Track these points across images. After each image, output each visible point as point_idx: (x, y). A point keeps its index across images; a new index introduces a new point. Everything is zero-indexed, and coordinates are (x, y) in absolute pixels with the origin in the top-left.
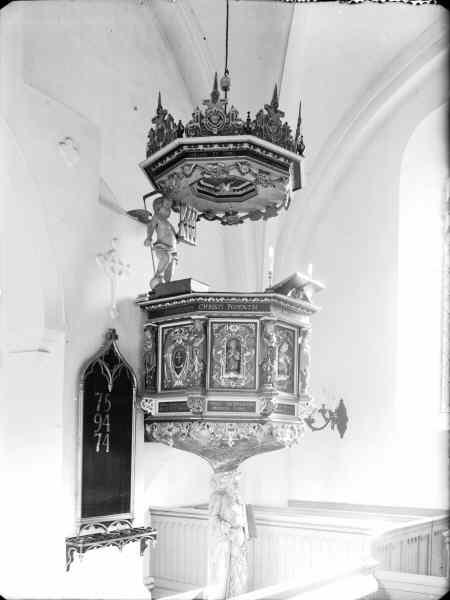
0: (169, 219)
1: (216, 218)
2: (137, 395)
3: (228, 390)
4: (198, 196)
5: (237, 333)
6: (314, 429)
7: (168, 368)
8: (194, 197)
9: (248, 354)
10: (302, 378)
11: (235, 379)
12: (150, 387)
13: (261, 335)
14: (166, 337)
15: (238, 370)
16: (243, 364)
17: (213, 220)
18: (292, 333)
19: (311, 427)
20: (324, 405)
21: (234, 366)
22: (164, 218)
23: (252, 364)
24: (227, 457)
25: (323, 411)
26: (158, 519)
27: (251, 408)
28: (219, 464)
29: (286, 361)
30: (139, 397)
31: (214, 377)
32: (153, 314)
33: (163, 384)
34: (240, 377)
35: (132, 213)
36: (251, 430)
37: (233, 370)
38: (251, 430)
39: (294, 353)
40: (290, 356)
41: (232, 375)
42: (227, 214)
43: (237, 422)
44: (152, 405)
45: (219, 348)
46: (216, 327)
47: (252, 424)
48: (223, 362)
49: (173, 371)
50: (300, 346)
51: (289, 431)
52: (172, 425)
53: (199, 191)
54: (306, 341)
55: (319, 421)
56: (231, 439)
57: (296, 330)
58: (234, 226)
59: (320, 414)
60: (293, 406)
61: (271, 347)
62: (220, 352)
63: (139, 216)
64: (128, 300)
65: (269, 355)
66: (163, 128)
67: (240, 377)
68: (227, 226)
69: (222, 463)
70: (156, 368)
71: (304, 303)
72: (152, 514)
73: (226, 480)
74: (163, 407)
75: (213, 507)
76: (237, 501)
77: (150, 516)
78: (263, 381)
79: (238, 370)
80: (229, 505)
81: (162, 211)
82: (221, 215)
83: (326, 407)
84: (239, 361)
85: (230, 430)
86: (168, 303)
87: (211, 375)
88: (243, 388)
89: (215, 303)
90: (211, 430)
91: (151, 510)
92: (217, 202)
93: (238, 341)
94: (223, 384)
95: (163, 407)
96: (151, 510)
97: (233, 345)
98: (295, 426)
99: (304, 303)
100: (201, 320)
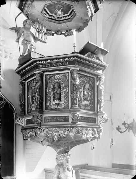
0: (30, 30)
1: (62, 34)
2: (16, 117)
3: (55, 110)
4: (49, 21)
5: (59, 79)
6: (121, 132)
7: (30, 102)
8: (47, 22)
9: (65, 90)
10: (99, 102)
11: (58, 104)
12: (23, 114)
13: (71, 79)
14: (28, 87)
15: (60, 99)
16: (63, 96)
17: (60, 35)
18: (92, 80)
19: (119, 131)
20: (124, 121)
21: (58, 97)
22: (28, 29)
23: (67, 96)
24: (64, 145)
25: (124, 124)
26: (48, 174)
27: (66, 119)
28: (59, 150)
29: (88, 93)
30: (16, 117)
31: (48, 104)
32: (22, 76)
33: (28, 110)
34: (62, 103)
35: (12, 29)
36: (67, 132)
37: (57, 99)
38: (67, 132)
39: (94, 90)
40: (91, 91)
41: (56, 102)
42: (67, 31)
43: (59, 127)
44: (22, 122)
45: (50, 88)
46: (48, 77)
47: (67, 129)
48: (52, 96)
49: (31, 104)
50: (98, 86)
51: (91, 132)
52: (29, 131)
53: (49, 18)
54: (101, 83)
55: (123, 129)
56: (56, 137)
57: (95, 77)
58: (70, 36)
59: (123, 125)
60: (95, 118)
61: (76, 84)
62: (50, 91)
63: (16, 29)
64: (11, 71)
65: (75, 88)
66: (73, 34)
67: (62, 103)
68: (67, 37)
69: (60, 150)
70: (25, 102)
71: (97, 61)
72: (45, 172)
73: (62, 159)
74: (28, 122)
75: (55, 173)
76: (68, 169)
77: (45, 173)
78: (73, 104)
79: (60, 99)
80: (64, 171)
81: (27, 26)
82: (64, 33)
83: (125, 122)
84: (60, 94)
85: (56, 132)
86: (27, 66)
87: (46, 102)
88: (63, 108)
89: (46, 64)
90: (45, 132)
91: (45, 170)
92: (60, 24)
93: (59, 83)
94: (52, 107)
95: (28, 122)
96: (45, 170)
97: (56, 86)
98: (95, 129)
99: (97, 61)
100: (38, 73)
